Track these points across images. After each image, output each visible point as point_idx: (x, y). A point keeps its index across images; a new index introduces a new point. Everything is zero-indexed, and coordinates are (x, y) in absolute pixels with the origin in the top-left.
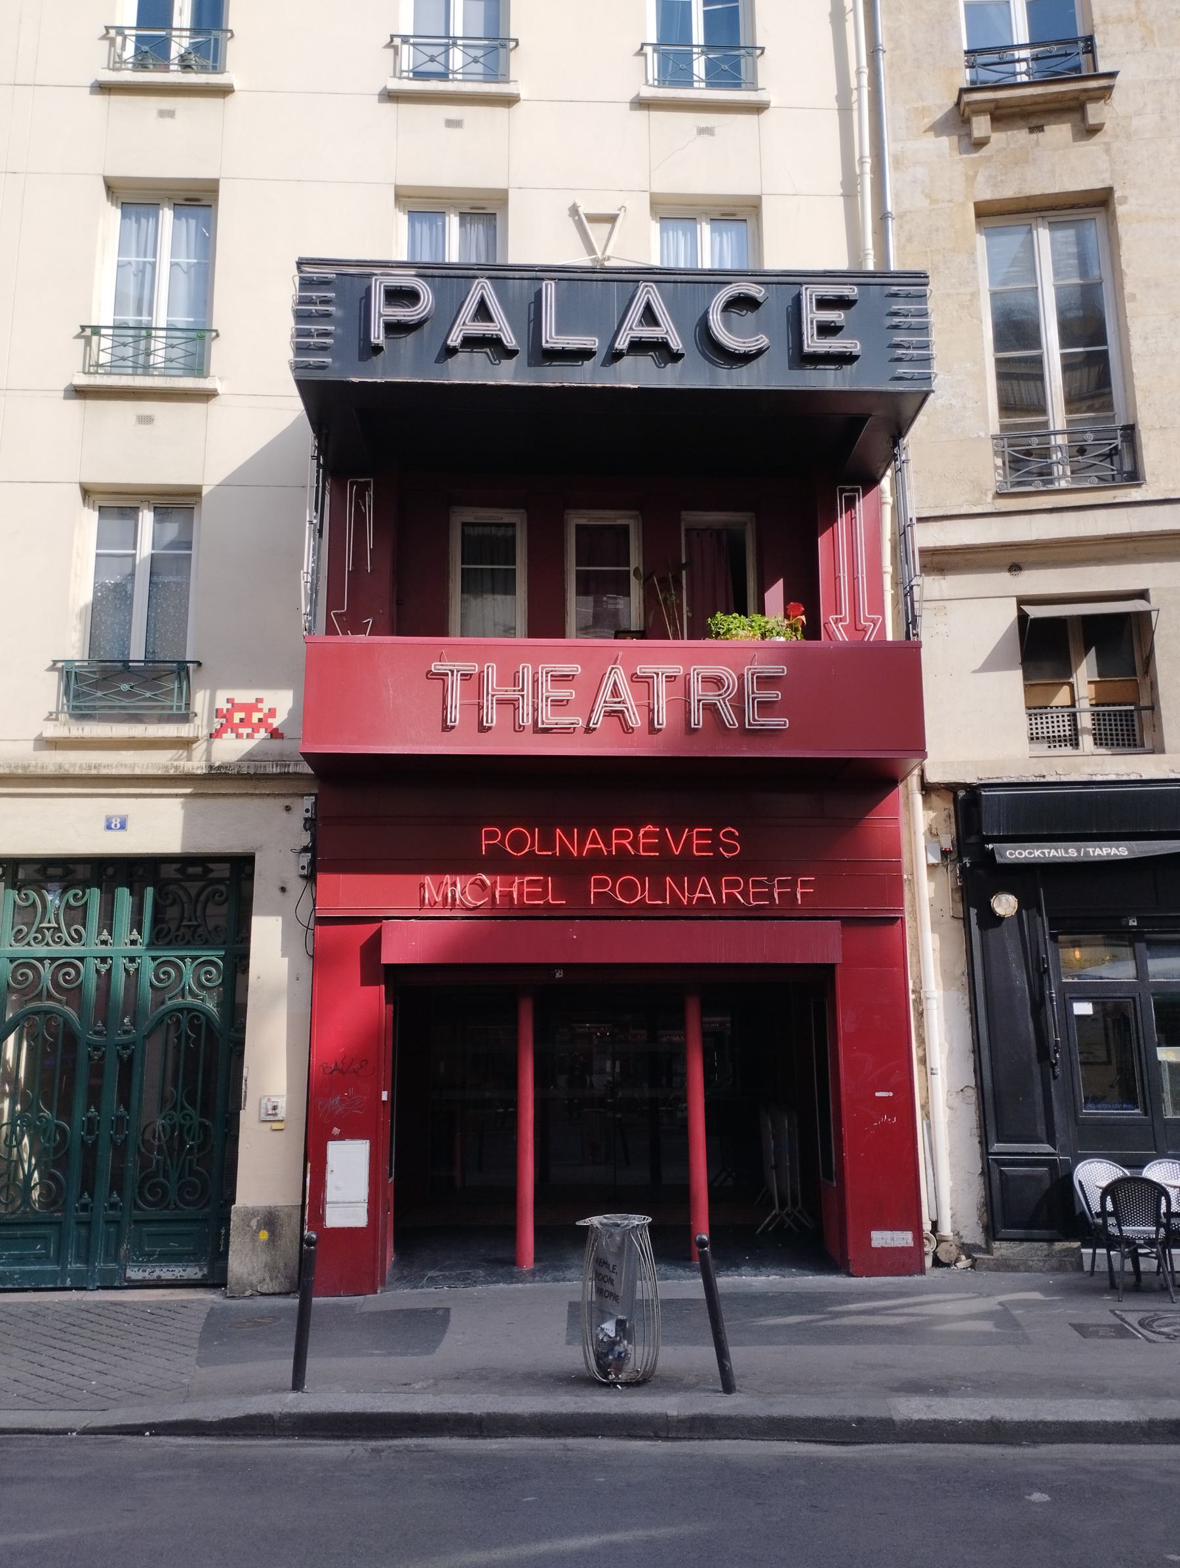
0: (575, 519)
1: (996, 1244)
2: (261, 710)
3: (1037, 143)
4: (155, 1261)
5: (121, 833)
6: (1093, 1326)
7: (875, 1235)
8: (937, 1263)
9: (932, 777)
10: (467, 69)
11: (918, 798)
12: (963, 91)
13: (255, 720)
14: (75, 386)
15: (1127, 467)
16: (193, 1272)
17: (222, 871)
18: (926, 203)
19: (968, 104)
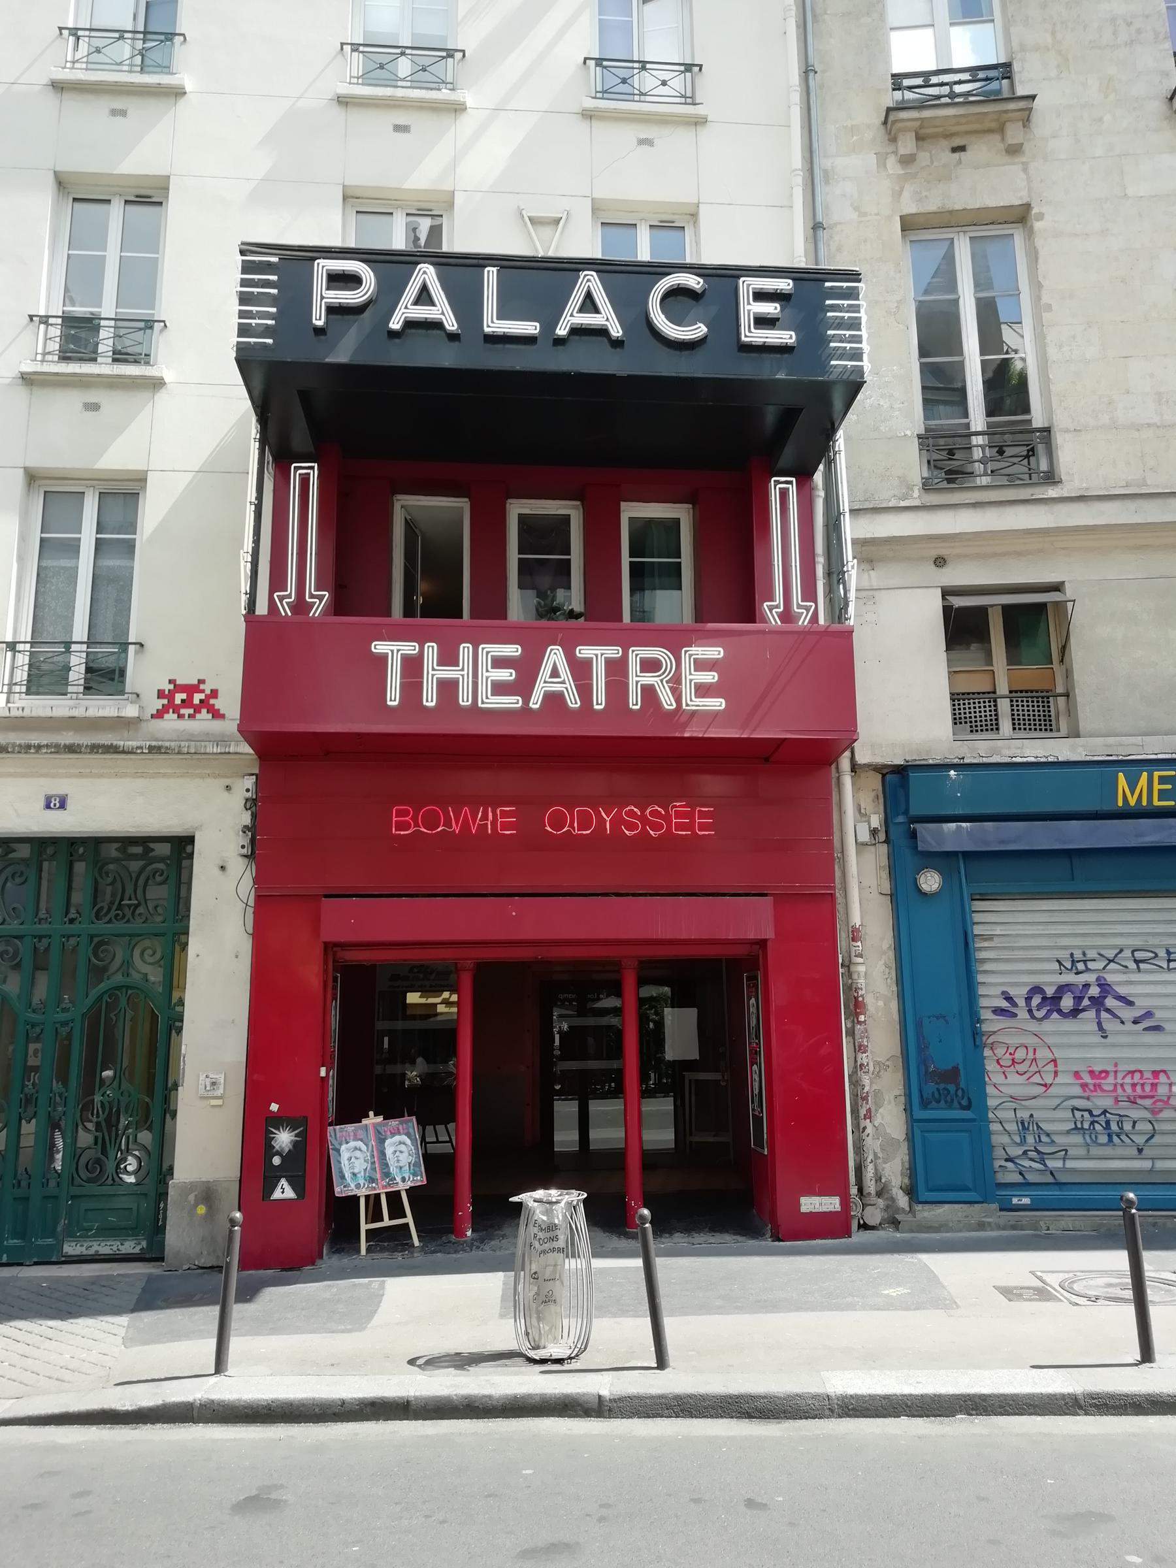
0: (516, 509)
1: (918, 1207)
2: (203, 691)
3: (960, 162)
4: (94, 1236)
5: (61, 812)
6: (1016, 1288)
7: (803, 1200)
8: (864, 1227)
9: (862, 758)
10: (415, 77)
11: (847, 780)
12: (889, 110)
13: (196, 701)
14: (22, 374)
15: (1044, 466)
16: (130, 1247)
17: (164, 849)
18: (855, 216)
19: (894, 122)
